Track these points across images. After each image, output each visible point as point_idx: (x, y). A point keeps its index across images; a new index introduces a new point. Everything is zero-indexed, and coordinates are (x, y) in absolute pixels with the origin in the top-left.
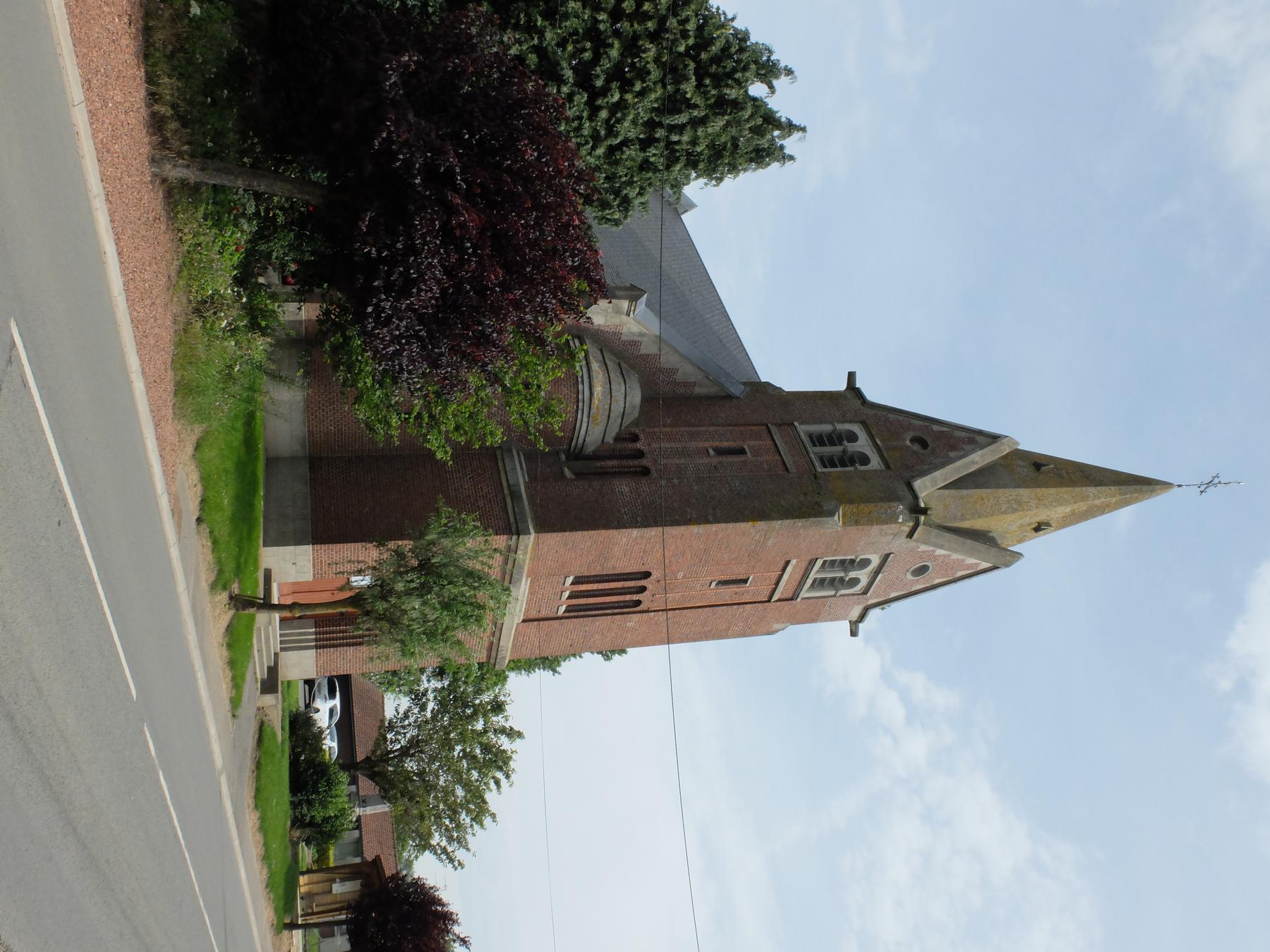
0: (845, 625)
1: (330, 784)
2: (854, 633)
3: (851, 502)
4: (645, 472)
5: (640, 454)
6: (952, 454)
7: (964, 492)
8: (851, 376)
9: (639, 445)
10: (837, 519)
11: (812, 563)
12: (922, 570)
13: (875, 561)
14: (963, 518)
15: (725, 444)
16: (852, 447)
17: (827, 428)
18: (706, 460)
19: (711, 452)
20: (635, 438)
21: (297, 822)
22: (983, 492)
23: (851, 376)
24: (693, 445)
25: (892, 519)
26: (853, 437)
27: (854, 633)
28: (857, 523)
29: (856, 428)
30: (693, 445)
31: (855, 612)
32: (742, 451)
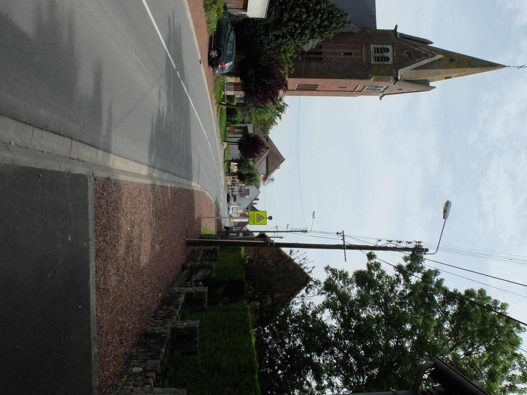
0: (379, 97)
1: (236, 114)
2: (380, 99)
3: (377, 75)
4: (321, 59)
5: (321, 53)
6: (417, 60)
7: (418, 71)
8: (396, 26)
9: (322, 50)
10: (372, 80)
11: (365, 87)
12: (401, 89)
13: (385, 87)
14: (416, 78)
15: (347, 51)
16: (386, 54)
17: (381, 46)
18: (339, 57)
19: (342, 54)
20: (321, 47)
21: (227, 120)
22: (425, 71)
23: (396, 26)
24: (337, 51)
25: (389, 80)
26: (388, 50)
27: (380, 99)
28: (377, 81)
29: (390, 47)
30: (337, 51)
31: (381, 95)
32: (351, 54)
